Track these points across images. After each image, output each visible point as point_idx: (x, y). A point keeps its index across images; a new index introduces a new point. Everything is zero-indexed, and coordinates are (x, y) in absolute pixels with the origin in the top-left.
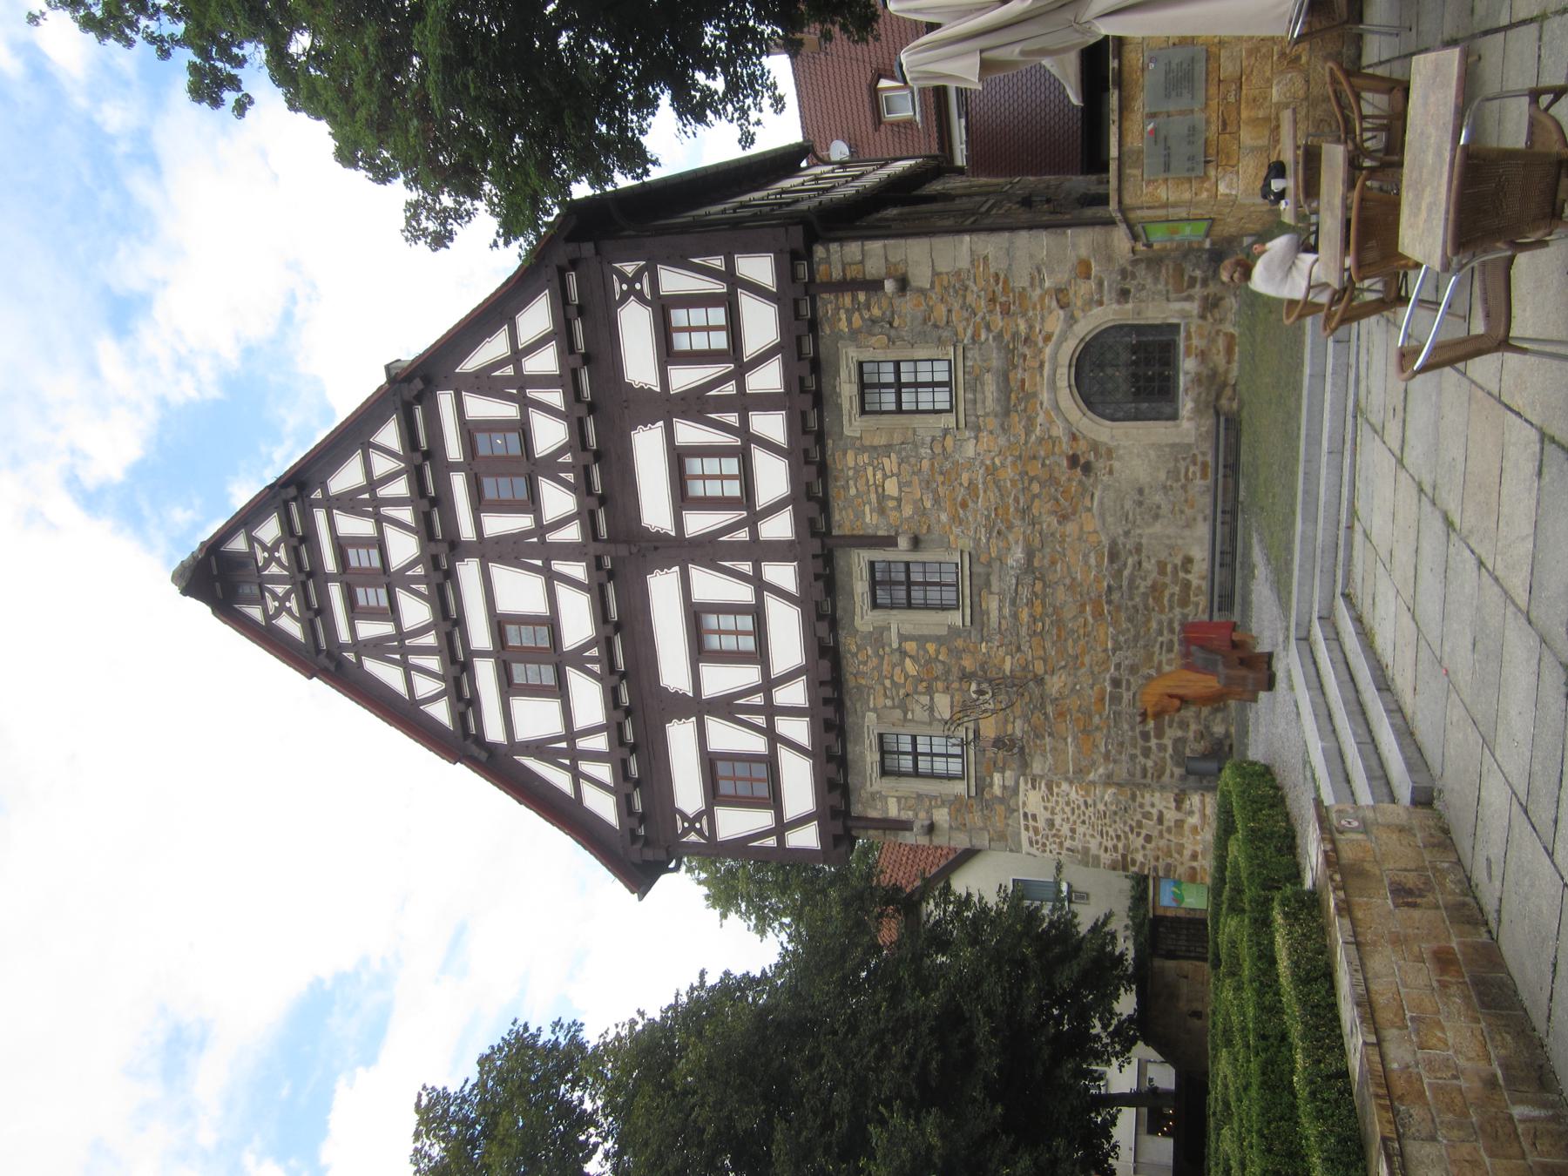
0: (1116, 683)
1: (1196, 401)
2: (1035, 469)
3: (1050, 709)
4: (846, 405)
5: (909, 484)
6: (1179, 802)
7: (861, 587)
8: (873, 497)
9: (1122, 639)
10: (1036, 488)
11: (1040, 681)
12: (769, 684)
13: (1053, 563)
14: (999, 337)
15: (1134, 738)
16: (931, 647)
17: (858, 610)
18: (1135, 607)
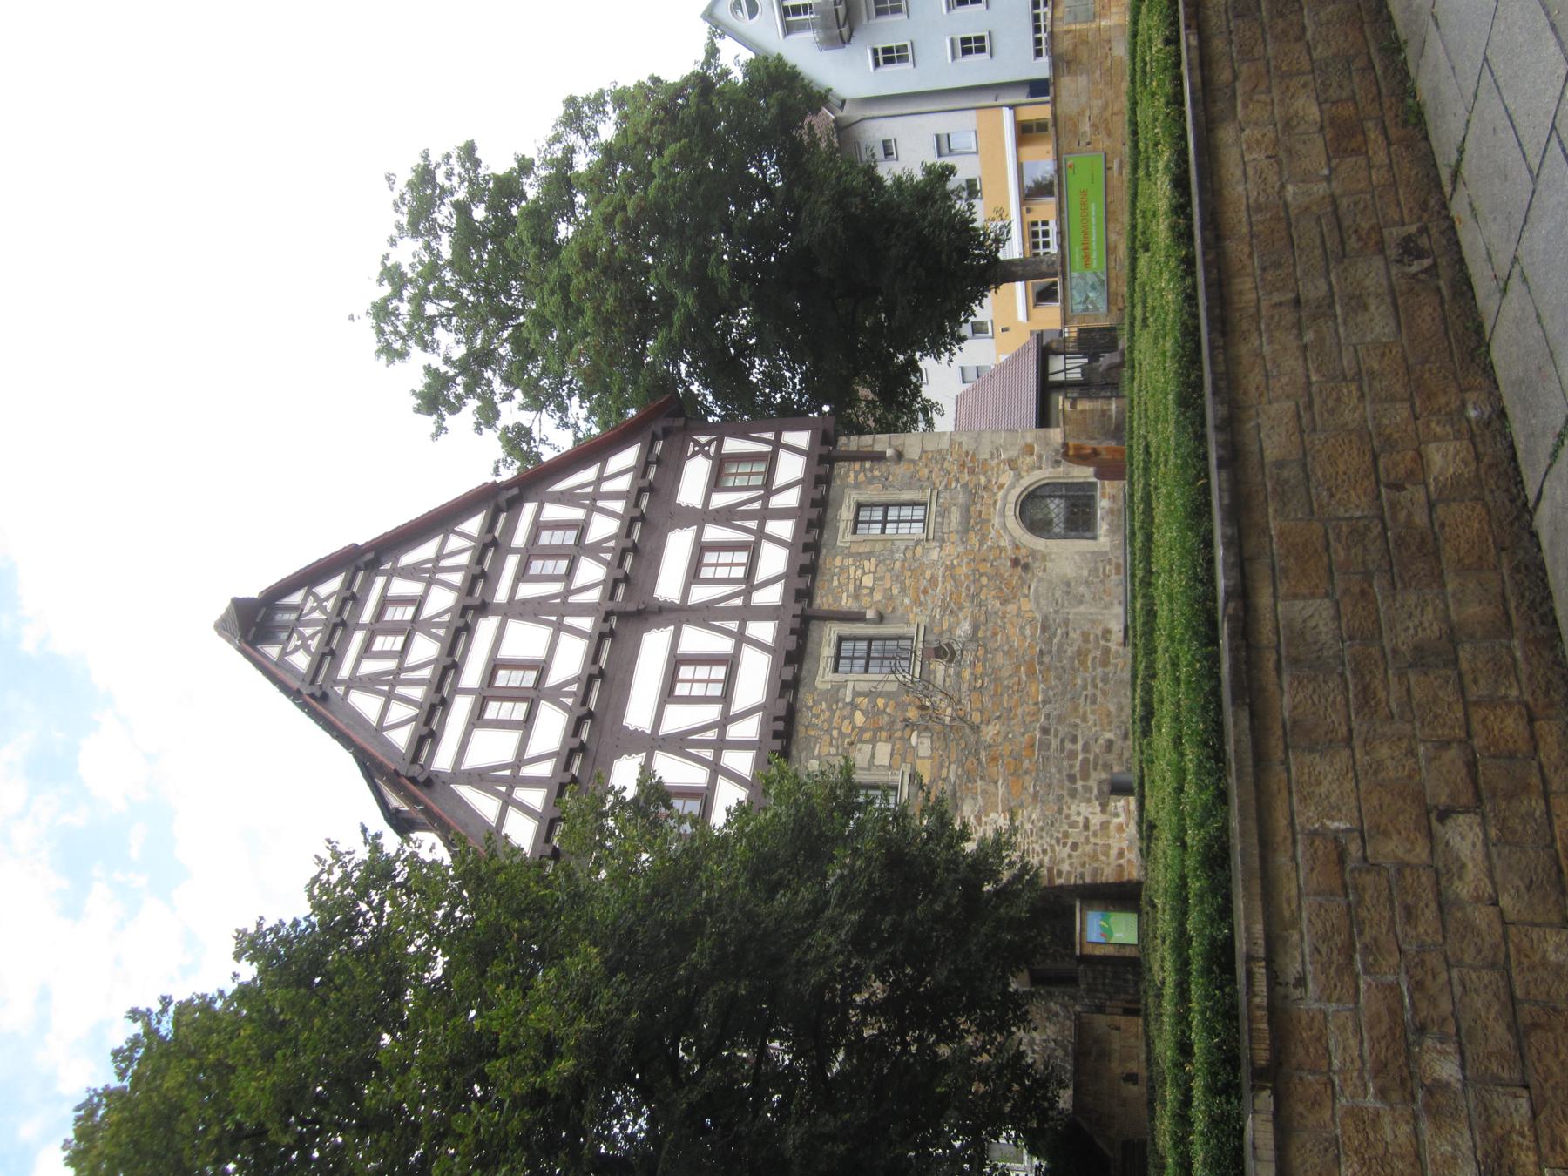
0: (1045, 731)
3: (983, 755)
4: (842, 526)
7: (828, 651)
8: (851, 587)
9: (1051, 693)
10: (984, 580)
11: (976, 729)
12: (726, 720)
13: (995, 634)
14: (965, 486)
15: (1060, 781)
16: (881, 702)
17: (821, 672)
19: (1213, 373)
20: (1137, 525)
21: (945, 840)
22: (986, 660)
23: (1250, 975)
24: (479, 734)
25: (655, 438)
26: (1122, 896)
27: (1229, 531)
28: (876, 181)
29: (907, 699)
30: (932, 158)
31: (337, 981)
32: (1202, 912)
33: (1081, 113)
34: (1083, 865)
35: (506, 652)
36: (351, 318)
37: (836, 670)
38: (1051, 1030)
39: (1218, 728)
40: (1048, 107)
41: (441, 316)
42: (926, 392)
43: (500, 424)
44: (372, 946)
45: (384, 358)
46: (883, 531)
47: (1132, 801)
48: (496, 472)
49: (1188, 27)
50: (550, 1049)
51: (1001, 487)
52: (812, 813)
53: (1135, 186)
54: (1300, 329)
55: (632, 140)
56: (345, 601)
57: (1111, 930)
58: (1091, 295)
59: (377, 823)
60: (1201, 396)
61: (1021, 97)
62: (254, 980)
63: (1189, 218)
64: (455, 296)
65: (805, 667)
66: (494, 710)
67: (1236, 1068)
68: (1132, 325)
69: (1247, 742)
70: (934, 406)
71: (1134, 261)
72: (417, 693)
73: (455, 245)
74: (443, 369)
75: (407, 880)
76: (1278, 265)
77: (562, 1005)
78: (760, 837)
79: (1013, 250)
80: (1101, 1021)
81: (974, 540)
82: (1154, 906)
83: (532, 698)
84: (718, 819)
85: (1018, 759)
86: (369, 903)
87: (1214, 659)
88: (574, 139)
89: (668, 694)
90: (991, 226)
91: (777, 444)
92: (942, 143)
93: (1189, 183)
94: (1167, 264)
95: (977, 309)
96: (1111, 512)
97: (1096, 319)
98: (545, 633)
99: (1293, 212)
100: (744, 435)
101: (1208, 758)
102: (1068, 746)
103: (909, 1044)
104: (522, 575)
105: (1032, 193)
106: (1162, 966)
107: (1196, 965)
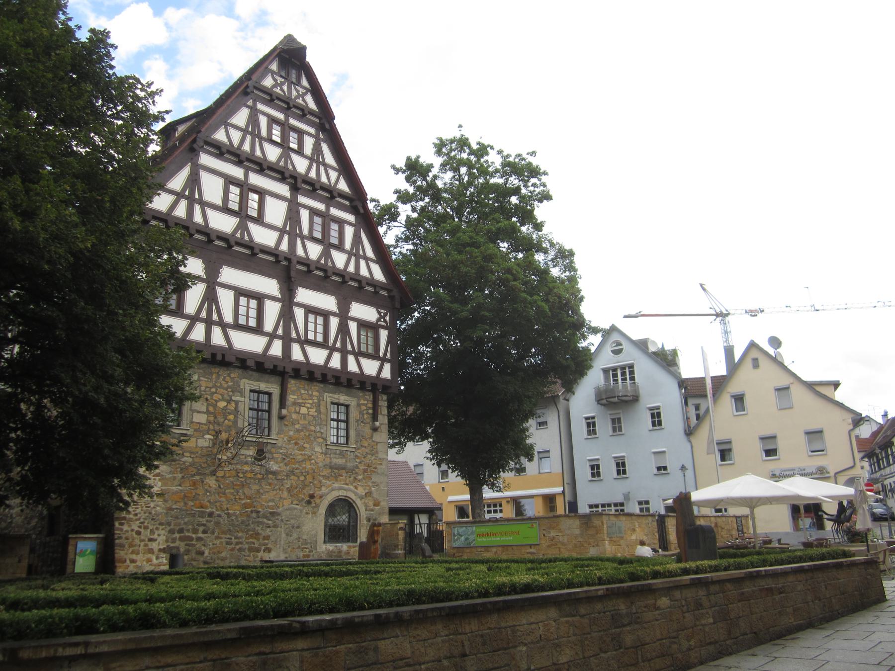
0: (211, 515)
1: (332, 551)
2: (309, 479)
3: (197, 478)
4: (336, 396)
5: (305, 418)
6: (163, 550)
7: (263, 386)
8: (300, 401)
9: (234, 518)
10: (302, 478)
11: (213, 473)
12: (224, 326)
13: (270, 484)
15: (180, 524)
16: (231, 417)
17: (251, 382)
18: (249, 525)
19: (427, 610)
20: (334, 567)
21: (147, 456)
22: (255, 479)
23: (76, 645)
24: (220, 182)
25: (389, 291)
26: (106, 562)
27: (339, 622)
28: (526, 419)
29: (233, 432)
30: (537, 449)
31: (73, 88)
32: (114, 614)
33: (560, 531)
34: (127, 539)
35: (269, 200)
36: (460, 126)
37: (251, 391)
38: (19, 520)
39: (225, 620)
40: (563, 513)
41: (460, 176)
42: (410, 444)
43: (399, 204)
44: (95, 111)
45: (438, 142)
46: (333, 420)
47: (166, 568)
48: (373, 200)
49: (607, 589)
50: (28, 215)
51: (356, 488)
52: (168, 376)
53: (522, 562)
54: (450, 657)
55: (551, 285)
56: (302, 110)
57: (84, 556)
58: (463, 538)
59: (169, 119)
60: (413, 604)
61: (568, 498)
62: (77, 39)
63: (509, 594)
64: (470, 184)
65: (254, 373)
66: (235, 191)
67: (14, 638)
68: (446, 562)
69: (217, 637)
70: (402, 450)
71: (482, 562)
72: (247, 147)
73: (496, 185)
74: (431, 175)
75: (136, 135)
76: (484, 644)
77: (55, 223)
78: (153, 345)
79: (488, 494)
80: (25, 551)
81: (326, 472)
82: (102, 583)
83: (241, 213)
84: (165, 320)
85: (194, 498)
86: (121, 111)
87: (265, 616)
88: (552, 254)
89: (240, 292)
90: (501, 481)
91: (383, 360)
92: (545, 454)
93: (529, 592)
94: (485, 582)
95: (456, 473)
96: (340, 552)
97: (449, 541)
98: (279, 223)
99: (512, 651)
100: (389, 341)
101: (207, 615)
102: (201, 529)
103: (16, 432)
104: (313, 212)
105: (516, 502)
106: (64, 590)
107: (82, 612)
